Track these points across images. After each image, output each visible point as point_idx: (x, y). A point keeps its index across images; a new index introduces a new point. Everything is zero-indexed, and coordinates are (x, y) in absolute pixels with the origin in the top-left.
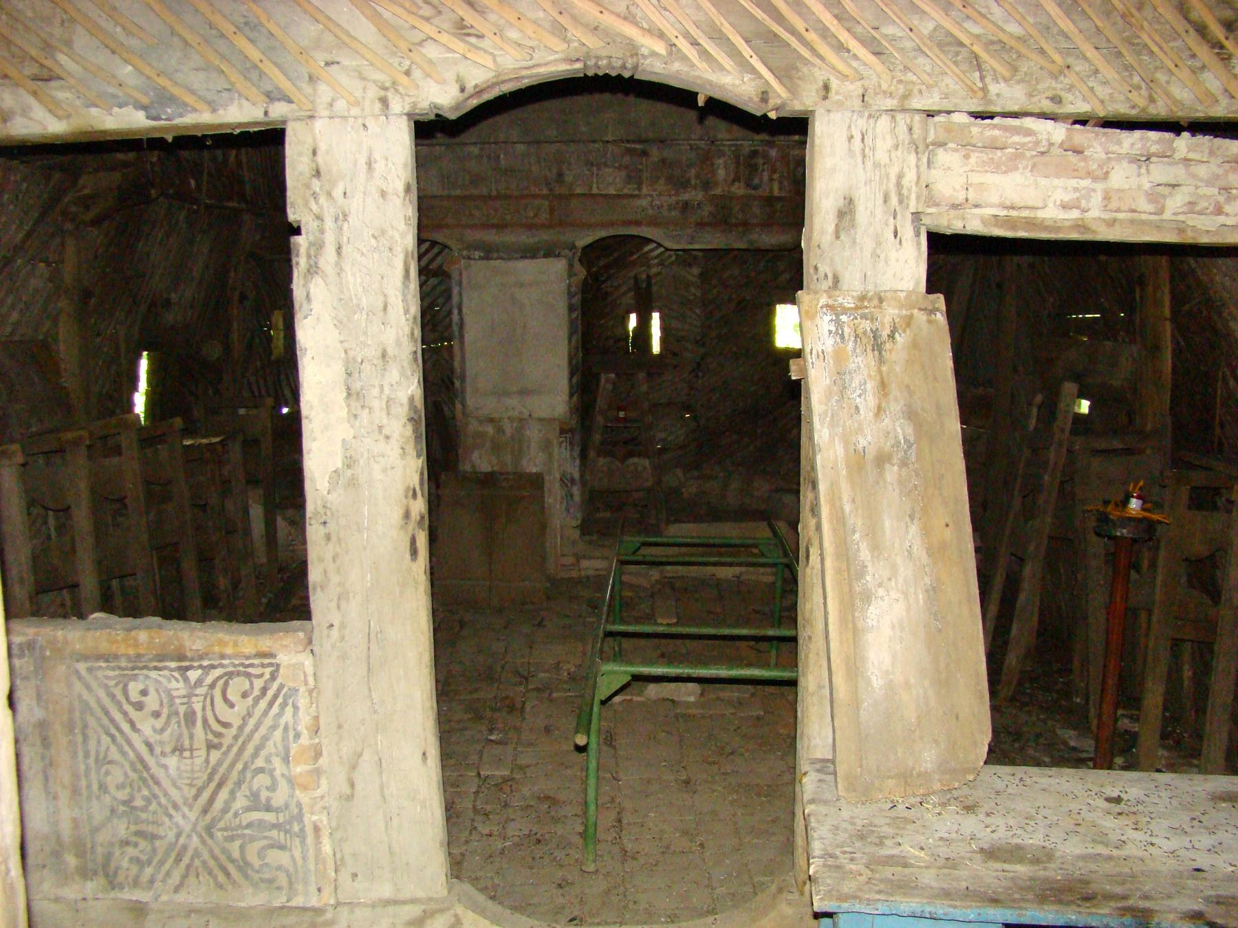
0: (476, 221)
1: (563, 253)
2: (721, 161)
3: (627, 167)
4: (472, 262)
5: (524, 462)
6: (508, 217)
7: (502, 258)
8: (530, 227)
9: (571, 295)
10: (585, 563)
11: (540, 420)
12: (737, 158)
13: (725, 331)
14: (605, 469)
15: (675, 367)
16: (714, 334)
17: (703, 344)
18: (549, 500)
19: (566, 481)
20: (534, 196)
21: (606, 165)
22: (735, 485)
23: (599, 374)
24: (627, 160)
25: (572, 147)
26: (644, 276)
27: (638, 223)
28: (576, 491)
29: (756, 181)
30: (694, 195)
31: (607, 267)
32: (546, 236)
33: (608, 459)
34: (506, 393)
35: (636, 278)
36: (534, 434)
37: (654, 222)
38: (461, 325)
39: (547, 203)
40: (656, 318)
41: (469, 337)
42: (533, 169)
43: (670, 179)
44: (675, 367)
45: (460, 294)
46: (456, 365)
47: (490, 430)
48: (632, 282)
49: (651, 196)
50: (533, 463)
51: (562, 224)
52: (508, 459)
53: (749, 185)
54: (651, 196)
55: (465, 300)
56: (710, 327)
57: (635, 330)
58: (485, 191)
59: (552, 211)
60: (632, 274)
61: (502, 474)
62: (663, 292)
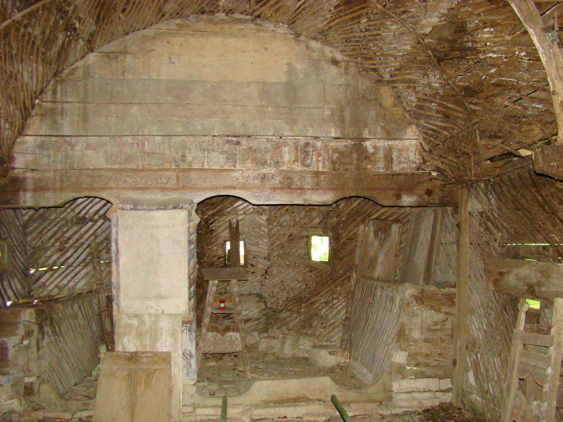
0: (128, 186)
1: (185, 206)
2: (286, 149)
3: (227, 152)
4: (125, 212)
5: (158, 344)
6: (149, 183)
7: (145, 210)
8: (164, 189)
9: (190, 234)
10: (199, 411)
11: (170, 315)
12: (297, 149)
13: (281, 252)
14: (212, 339)
15: (253, 273)
16: (275, 254)
17: (269, 260)
18: (174, 370)
19: (186, 355)
20: (167, 170)
21: (213, 150)
22: (289, 342)
23: (208, 281)
24: (226, 147)
25: (192, 139)
26: (235, 221)
27: (234, 188)
28: (193, 362)
29: (308, 162)
30: (269, 170)
31: (213, 215)
32: (174, 196)
33: (214, 333)
34: (147, 298)
35: (230, 221)
36: (165, 324)
37: (244, 187)
38: (118, 252)
39: (175, 174)
40: (242, 243)
41: (122, 260)
42: (166, 152)
43: (254, 160)
44: (253, 273)
45: (117, 233)
46: (114, 279)
47: (135, 322)
48: (228, 223)
49: (242, 170)
50: (163, 347)
51: (184, 188)
52: (148, 342)
53: (304, 164)
54: (242, 170)
55: (120, 236)
56: (273, 249)
57: (229, 251)
58: (134, 166)
59: (178, 177)
60: (228, 219)
61: (143, 353)
62: (246, 229)
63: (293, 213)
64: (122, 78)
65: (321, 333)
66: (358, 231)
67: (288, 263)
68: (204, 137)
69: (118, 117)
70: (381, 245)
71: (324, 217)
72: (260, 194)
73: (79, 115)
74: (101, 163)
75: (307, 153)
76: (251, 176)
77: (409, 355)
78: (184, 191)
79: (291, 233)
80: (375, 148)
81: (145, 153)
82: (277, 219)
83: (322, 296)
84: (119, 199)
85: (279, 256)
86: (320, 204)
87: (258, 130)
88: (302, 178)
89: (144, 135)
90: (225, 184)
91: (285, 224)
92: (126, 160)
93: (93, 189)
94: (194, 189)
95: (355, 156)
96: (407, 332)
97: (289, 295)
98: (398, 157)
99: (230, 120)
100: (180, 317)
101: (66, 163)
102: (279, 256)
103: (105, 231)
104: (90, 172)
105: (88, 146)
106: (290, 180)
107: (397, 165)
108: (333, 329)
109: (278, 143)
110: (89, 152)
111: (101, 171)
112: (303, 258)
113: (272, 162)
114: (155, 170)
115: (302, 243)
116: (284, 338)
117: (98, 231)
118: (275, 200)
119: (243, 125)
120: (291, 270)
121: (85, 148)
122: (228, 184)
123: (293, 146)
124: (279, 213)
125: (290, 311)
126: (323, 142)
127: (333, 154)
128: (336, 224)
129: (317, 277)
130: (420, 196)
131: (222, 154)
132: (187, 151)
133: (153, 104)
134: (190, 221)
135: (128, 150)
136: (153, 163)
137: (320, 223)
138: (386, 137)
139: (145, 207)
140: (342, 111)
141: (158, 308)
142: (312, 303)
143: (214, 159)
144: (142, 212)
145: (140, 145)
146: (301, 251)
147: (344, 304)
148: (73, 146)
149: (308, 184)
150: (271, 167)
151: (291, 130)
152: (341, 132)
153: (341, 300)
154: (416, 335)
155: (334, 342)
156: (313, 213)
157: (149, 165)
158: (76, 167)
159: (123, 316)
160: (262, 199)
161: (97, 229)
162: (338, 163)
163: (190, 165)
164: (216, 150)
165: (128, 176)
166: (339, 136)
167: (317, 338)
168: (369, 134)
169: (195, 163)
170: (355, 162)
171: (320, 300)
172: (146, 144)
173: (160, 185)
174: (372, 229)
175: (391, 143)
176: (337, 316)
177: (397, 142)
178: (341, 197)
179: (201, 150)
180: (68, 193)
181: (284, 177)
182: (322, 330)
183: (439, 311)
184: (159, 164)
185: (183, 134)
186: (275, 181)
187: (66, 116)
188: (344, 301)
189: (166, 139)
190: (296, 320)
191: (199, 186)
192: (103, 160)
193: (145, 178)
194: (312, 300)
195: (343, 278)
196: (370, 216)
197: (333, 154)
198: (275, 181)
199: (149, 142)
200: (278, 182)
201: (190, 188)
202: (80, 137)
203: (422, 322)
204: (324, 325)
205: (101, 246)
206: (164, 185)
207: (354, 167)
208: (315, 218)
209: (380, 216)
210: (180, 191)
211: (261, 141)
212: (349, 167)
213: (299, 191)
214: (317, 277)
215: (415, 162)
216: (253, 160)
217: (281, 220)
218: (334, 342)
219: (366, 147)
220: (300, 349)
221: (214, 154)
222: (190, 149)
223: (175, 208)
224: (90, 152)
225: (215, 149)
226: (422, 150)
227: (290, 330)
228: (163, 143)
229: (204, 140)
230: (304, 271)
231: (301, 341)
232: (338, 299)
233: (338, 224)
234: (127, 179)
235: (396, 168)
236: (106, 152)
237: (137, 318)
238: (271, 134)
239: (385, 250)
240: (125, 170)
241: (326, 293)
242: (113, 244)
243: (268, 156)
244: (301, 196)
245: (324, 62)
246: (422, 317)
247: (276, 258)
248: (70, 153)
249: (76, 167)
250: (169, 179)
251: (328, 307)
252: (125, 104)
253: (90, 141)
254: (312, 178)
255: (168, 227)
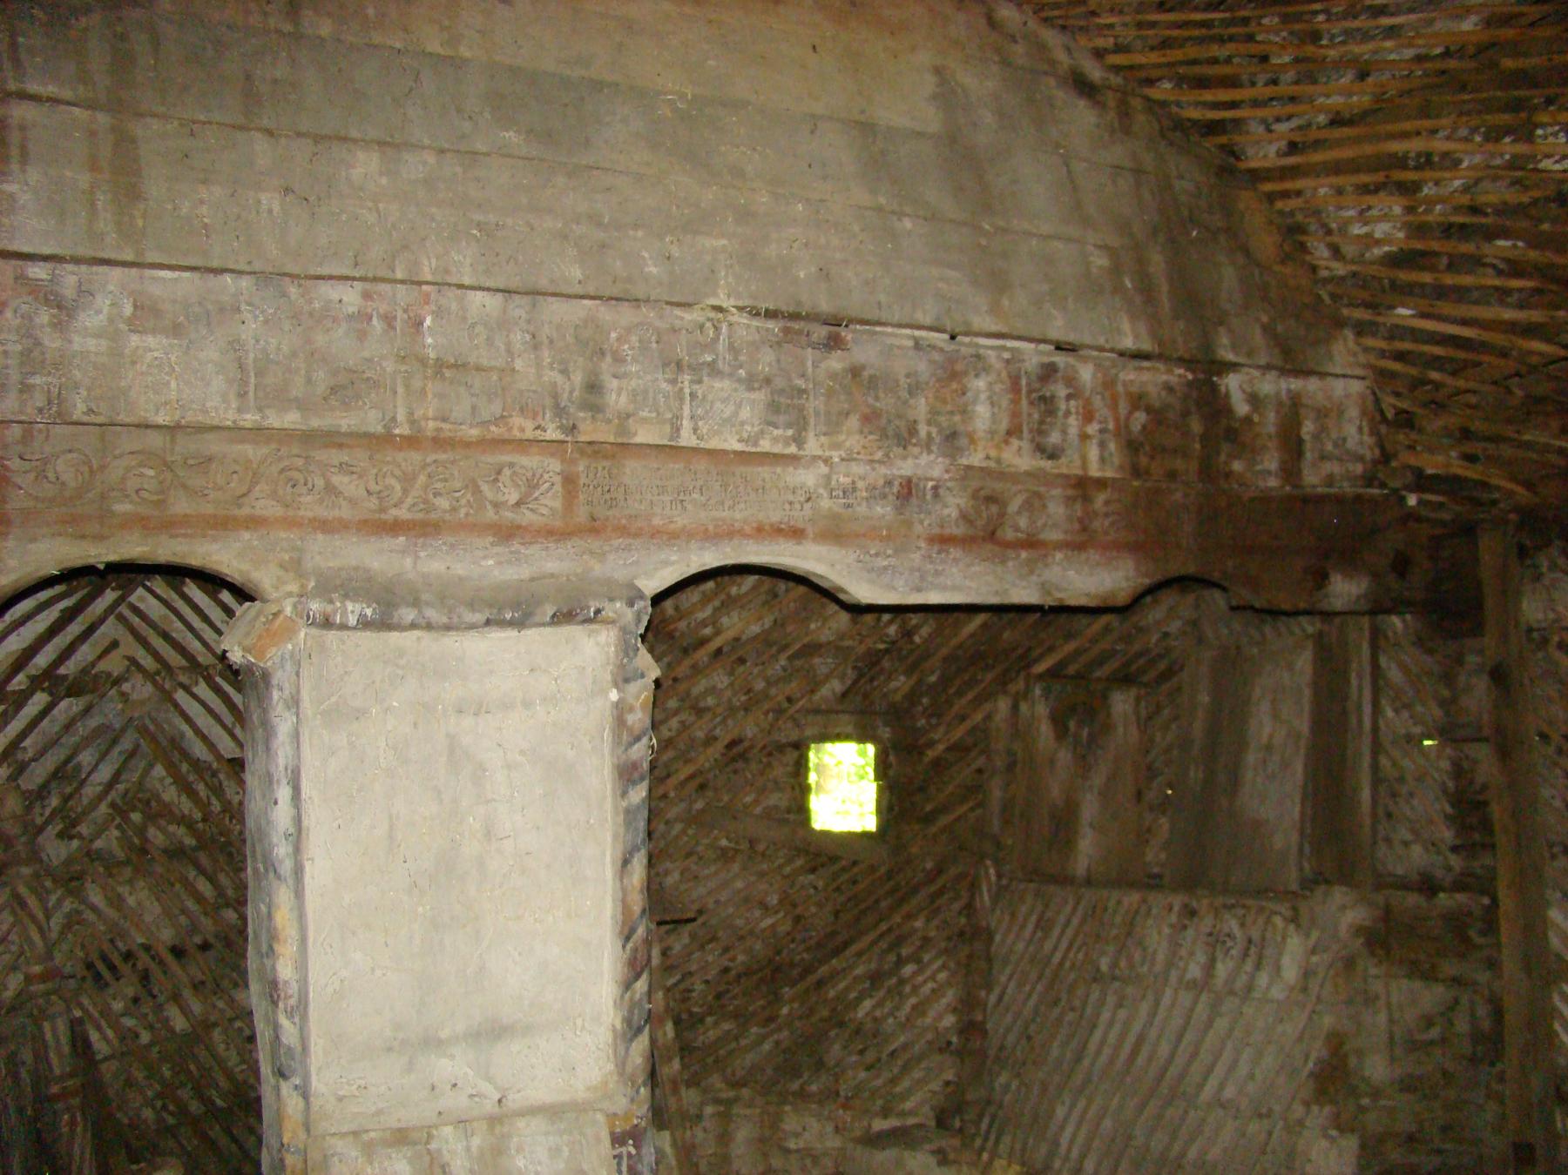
0: (345, 512)
2: (981, 383)
3: (768, 381)
4: (331, 636)
6: (443, 503)
7: (429, 627)
8: (507, 533)
12: (1015, 386)
13: (699, 805)
16: (673, 813)
20: (523, 445)
21: (714, 370)
29: (1054, 438)
30: (926, 465)
34: (432, 1043)
38: (297, 837)
41: (317, 874)
45: (296, 735)
51: (594, 528)
53: (1040, 449)
54: (827, 461)
56: (665, 796)
58: (372, 422)
59: (569, 481)
63: (742, 661)
64: (288, 27)
65: (858, 1089)
66: (988, 717)
67: (724, 842)
68: (678, 312)
69: (287, 190)
70: (1084, 763)
71: (861, 676)
72: (893, 561)
73: (94, 167)
74: (215, 401)
75: (1047, 404)
76: (860, 484)
77: (1363, 1146)
78: (595, 544)
79: (735, 734)
80: (1254, 399)
81: (423, 361)
82: (682, 687)
83: (859, 954)
84: (301, 575)
85: (693, 819)
86: (1093, 604)
87: (882, 298)
88: (1034, 503)
89: (420, 283)
90: (761, 516)
91: (710, 701)
92: (333, 390)
93: (171, 526)
94: (637, 535)
95: (1196, 426)
96: (1353, 1061)
97: (733, 959)
98: (1316, 437)
99: (771, 251)
100: (600, 1117)
101: (25, 389)
102: (693, 819)
103: (54, 742)
104: (155, 440)
105: (146, 314)
106: (994, 509)
107: (1314, 465)
108: (906, 1068)
109: (952, 359)
110: (151, 340)
111: (210, 436)
112: (783, 822)
113: (934, 431)
114: (467, 445)
115: (779, 771)
116: (725, 1117)
117: (27, 743)
118: (944, 588)
119: (824, 274)
120: (736, 867)
121: (130, 321)
122: (775, 516)
123: (1004, 374)
124: (688, 662)
125: (736, 1015)
126: (1098, 366)
127: (1130, 413)
128: (906, 697)
129: (838, 889)
130: (1376, 576)
131: (751, 389)
132: (606, 364)
133: (442, 151)
134: (624, 678)
135: (338, 342)
136: (460, 410)
137: (844, 695)
138: (1280, 363)
139: (432, 614)
140: (1141, 262)
141: (486, 1087)
142: (820, 984)
143: (718, 405)
144: (407, 639)
145: (398, 324)
146: (776, 799)
147: (942, 976)
148: (64, 310)
149: (1055, 525)
150: (930, 452)
151: (995, 309)
152: (1153, 335)
153: (930, 962)
154: (1377, 1068)
155: (911, 1113)
156: (817, 660)
157: (444, 420)
158: (79, 411)
159: (339, 1145)
160: (900, 583)
161: (23, 735)
162: (1147, 448)
163: (622, 430)
164: (727, 369)
165: (344, 468)
166: (1146, 345)
167: (845, 1106)
168: (1234, 348)
169: (644, 420)
170: (1197, 446)
171: (851, 968)
172: (428, 322)
173: (490, 515)
174: (1042, 709)
175: (1295, 384)
176: (919, 1022)
177: (1312, 385)
178: (1159, 577)
179: (666, 365)
180: (33, 540)
181: (975, 496)
182: (863, 1075)
183: (1429, 975)
184: (485, 415)
185: (591, 290)
186: (946, 511)
187: (24, 158)
188: (944, 967)
189: (519, 308)
190: (758, 1048)
191: (657, 521)
192: (218, 383)
193: (422, 479)
194: (823, 970)
195: (933, 888)
196: (1028, 666)
197: (1130, 413)
198: (946, 511)
199: (438, 314)
200: (955, 514)
201: (623, 531)
202: (104, 269)
203: (1391, 1021)
204: (870, 1056)
205: (37, 810)
206: (509, 515)
207: (1194, 466)
208: (828, 677)
209: (1062, 664)
210: (576, 541)
211: (891, 347)
212: (1179, 464)
213: (1024, 555)
214: (838, 889)
215: (1361, 459)
216: (866, 419)
217: (695, 691)
218: (911, 1113)
219: (1227, 395)
220: (788, 1151)
221: (717, 385)
222: (619, 359)
223: (565, 617)
224: (153, 345)
225: (720, 364)
226: (1378, 418)
227: (737, 1084)
228: (504, 324)
229: (678, 323)
230: (788, 870)
231: (791, 1123)
232: (919, 961)
233: (912, 697)
234: (337, 480)
235: (1312, 478)
236: (235, 345)
237: (408, 1151)
238: (928, 321)
239: (1098, 780)
240: (333, 439)
241: (874, 943)
242: (284, 793)
243: (920, 407)
244: (1032, 572)
245: (1052, 82)
246: (1389, 1005)
247: (678, 827)
248: (52, 342)
249: (79, 412)
250: (532, 485)
251: (881, 993)
252: (318, 139)
253: (156, 290)
254: (1069, 501)
255: (528, 704)
